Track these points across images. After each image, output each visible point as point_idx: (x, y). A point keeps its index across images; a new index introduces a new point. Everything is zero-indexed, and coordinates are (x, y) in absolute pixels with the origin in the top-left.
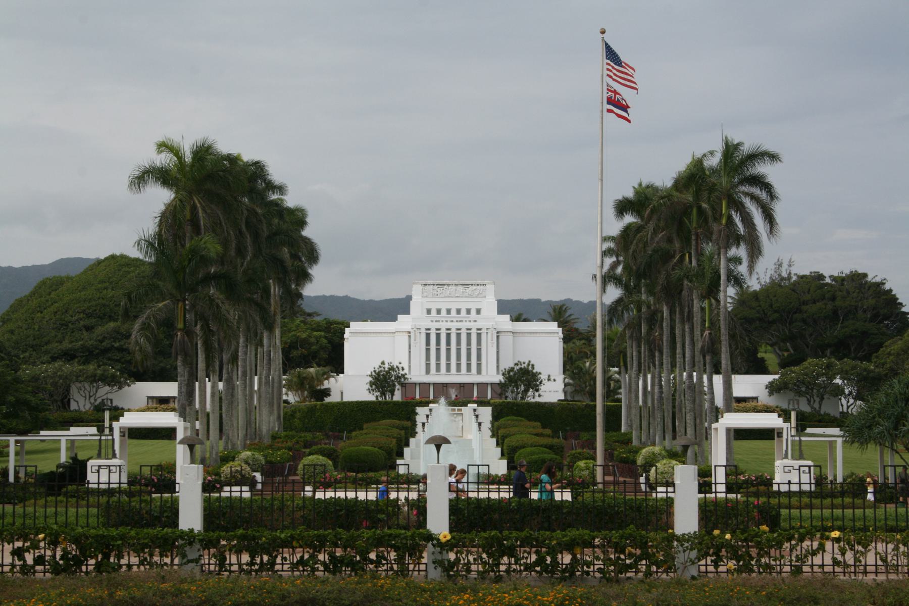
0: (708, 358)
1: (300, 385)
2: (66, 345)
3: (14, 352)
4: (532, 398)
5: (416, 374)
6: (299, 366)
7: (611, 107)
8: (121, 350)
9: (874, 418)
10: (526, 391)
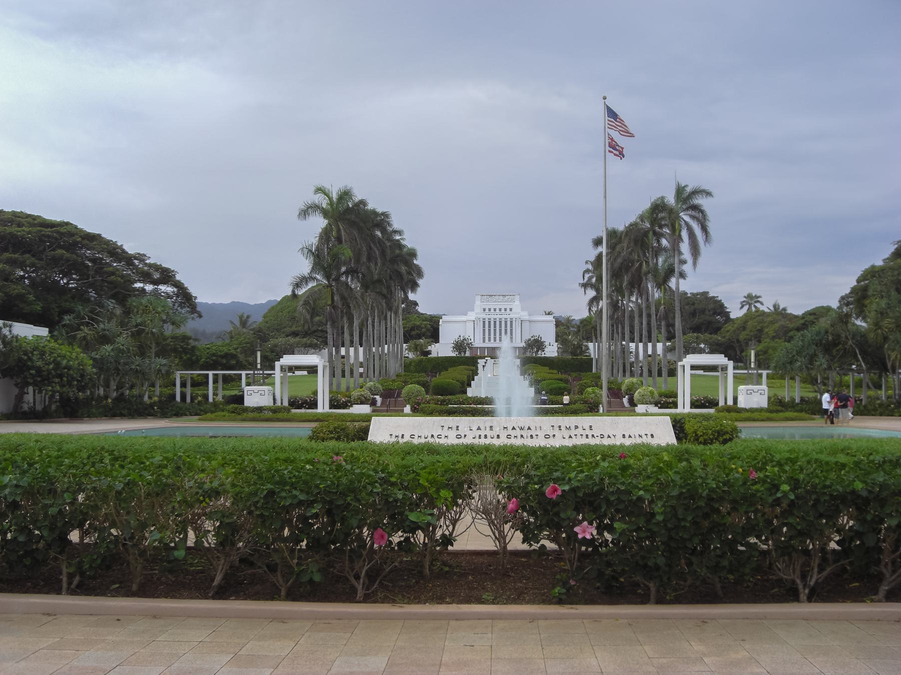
0: (663, 323)
1: (415, 348)
2: (294, 329)
3: (267, 332)
4: (541, 354)
5: (478, 343)
6: (415, 339)
7: (611, 149)
8: (322, 331)
9: (794, 356)
10: (538, 351)
